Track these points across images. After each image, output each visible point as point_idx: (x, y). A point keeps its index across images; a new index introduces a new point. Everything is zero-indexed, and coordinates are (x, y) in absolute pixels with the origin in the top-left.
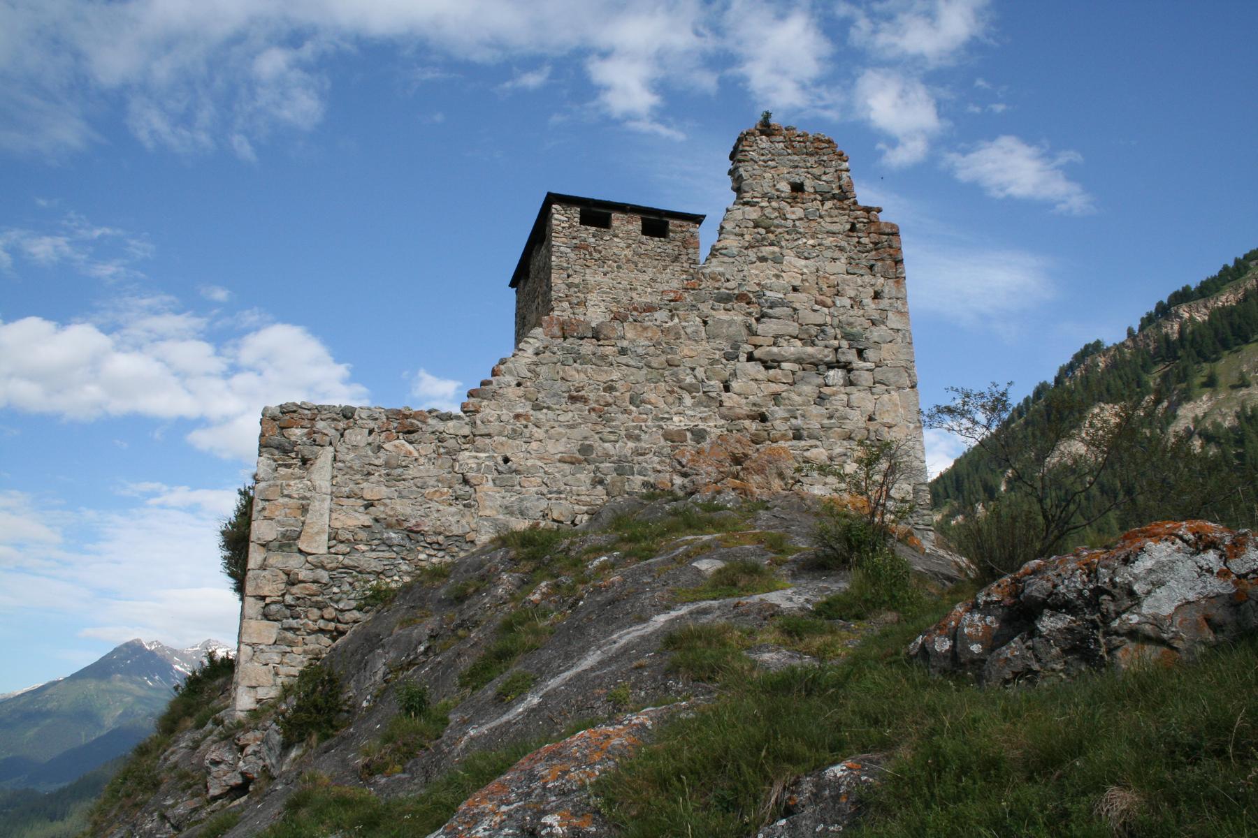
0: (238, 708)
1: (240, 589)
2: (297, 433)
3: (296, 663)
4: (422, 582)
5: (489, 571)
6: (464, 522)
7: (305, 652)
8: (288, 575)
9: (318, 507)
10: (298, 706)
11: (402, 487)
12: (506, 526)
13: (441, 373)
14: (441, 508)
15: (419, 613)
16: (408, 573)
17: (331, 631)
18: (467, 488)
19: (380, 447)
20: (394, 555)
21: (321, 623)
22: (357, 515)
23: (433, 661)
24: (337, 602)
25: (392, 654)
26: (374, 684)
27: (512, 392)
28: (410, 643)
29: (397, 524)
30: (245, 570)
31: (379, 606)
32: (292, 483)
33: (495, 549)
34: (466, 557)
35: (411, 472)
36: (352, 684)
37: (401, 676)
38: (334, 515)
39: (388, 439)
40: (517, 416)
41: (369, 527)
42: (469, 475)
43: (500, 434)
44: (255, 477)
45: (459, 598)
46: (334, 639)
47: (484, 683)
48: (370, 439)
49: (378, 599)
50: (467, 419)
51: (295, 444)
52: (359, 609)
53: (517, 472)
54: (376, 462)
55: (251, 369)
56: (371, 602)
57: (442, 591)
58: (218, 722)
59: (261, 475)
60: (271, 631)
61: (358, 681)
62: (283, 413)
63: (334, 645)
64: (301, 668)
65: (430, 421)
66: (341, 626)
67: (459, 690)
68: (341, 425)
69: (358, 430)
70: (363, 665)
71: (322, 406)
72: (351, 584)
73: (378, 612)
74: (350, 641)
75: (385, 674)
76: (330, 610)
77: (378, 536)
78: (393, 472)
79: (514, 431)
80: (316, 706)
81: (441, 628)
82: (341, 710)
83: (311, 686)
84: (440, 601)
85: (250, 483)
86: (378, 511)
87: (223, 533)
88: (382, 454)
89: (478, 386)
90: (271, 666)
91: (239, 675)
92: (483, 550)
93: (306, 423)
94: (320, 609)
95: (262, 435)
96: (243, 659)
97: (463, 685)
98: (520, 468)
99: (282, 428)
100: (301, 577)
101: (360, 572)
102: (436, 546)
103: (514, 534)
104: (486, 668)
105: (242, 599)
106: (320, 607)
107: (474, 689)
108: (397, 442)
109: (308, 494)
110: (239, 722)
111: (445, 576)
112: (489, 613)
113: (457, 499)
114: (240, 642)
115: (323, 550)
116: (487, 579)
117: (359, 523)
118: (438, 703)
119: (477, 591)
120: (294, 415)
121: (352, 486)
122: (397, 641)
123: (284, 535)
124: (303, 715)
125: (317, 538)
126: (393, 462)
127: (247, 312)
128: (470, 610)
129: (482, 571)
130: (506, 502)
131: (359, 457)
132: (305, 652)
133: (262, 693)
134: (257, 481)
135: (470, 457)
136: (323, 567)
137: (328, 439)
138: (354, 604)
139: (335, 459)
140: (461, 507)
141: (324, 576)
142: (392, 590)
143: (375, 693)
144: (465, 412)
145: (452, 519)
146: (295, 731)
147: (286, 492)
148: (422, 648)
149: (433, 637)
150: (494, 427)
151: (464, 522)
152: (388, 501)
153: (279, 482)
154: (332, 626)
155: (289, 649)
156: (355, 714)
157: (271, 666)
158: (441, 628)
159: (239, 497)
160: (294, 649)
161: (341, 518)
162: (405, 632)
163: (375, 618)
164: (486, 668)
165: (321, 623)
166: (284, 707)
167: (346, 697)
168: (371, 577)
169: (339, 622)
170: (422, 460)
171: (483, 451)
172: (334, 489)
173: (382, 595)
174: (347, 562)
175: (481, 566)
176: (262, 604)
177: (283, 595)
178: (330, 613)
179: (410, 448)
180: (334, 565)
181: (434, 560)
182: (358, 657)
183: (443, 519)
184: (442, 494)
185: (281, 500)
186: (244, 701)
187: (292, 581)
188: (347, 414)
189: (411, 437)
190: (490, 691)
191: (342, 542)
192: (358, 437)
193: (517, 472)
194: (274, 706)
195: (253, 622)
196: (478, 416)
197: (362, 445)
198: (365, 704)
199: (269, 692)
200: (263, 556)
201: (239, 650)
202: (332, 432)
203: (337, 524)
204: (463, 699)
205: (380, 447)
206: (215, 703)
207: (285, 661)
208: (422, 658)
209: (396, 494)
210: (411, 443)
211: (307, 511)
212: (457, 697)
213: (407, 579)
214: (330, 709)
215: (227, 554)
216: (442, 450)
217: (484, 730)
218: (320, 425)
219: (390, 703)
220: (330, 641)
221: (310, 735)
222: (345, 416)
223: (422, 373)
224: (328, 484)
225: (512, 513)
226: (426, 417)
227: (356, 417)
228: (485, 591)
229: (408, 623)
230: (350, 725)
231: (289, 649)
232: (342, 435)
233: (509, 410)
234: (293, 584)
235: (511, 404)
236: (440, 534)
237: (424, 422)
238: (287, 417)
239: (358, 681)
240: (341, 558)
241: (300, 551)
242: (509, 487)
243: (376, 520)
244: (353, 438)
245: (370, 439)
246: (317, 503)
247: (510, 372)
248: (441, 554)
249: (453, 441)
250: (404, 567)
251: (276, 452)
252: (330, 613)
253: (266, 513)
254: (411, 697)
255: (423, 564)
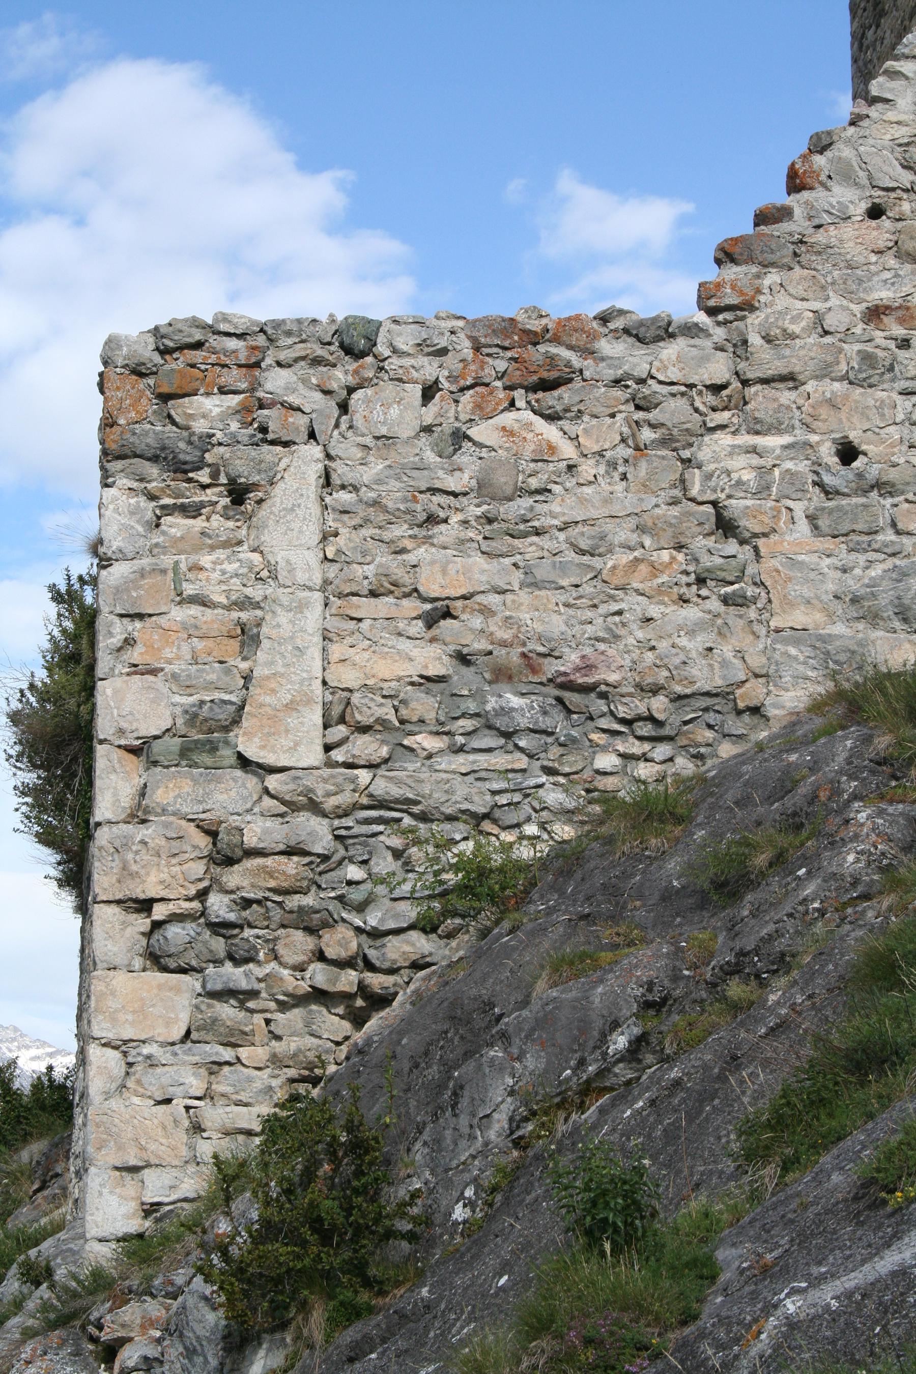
0: (92, 1231)
1: (76, 877)
2: (209, 411)
3: (250, 1098)
4: (609, 841)
5: (813, 799)
6: (726, 651)
7: (276, 1060)
8: (213, 834)
9: (286, 630)
10: (266, 1223)
11: (532, 553)
12: (856, 655)
13: (624, 178)
14: (654, 611)
15: (607, 934)
16: (567, 814)
17: (346, 997)
18: (732, 547)
19: (459, 438)
20: (522, 762)
21: (319, 975)
22: (404, 645)
23: (655, 1080)
24: (361, 908)
25: (533, 1062)
26: (482, 1153)
27: (856, 238)
28: (584, 1026)
29: (523, 665)
30: (87, 829)
31: (486, 917)
32: (206, 560)
33: (828, 731)
34: (741, 759)
35: (559, 508)
36: (419, 1153)
37: (561, 1128)
38: (337, 651)
39: (483, 413)
40: (875, 314)
41: (440, 679)
42: (736, 506)
43: (824, 373)
44: (95, 547)
45: (727, 886)
46: (358, 1020)
47: (817, 1148)
48: (429, 414)
49: (481, 895)
50: (719, 333)
51: (206, 442)
52: (427, 926)
53: (883, 487)
54: (452, 483)
55: (50, 208)
56: (461, 905)
57: (673, 865)
58: (38, 1275)
59: (114, 543)
60: (170, 1003)
61: (437, 1144)
62: (164, 352)
63: (359, 1037)
64: (266, 1109)
65: (606, 347)
66: (376, 981)
67: (740, 1171)
68: (340, 377)
69: (389, 389)
70: (447, 1097)
71: (278, 324)
72: (397, 854)
73: (484, 933)
74: (405, 1026)
75: (515, 1123)
76: (343, 932)
77: (472, 707)
78: (505, 514)
79: (867, 359)
80: (316, 1223)
81: (676, 977)
82: (390, 1234)
83: (299, 1163)
84: (667, 896)
85: (83, 565)
86: (465, 630)
87: (15, 718)
88: (466, 457)
89: (746, 228)
90: (179, 1104)
91: (87, 1134)
92: (792, 735)
93: (234, 377)
94: (310, 931)
95: (108, 423)
96: (96, 1085)
97: (754, 1155)
98: (892, 475)
99: (165, 398)
100: (251, 840)
101: (423, 817)
102: (645, 729)
103: (884, 680)
104: (819, 1102)
105: (83, 909)
106: (312, 924)
107: (786, 1168)
108: (508, 419)
109: (256, 592)
110: (97, 1274)
111: (679, 820)
112: (819, 928)
113: (701, 581)
114: (83, 1038)
115: (313, 755)
116: (808, 824)
117: (412, 671)
118: (680, 1211)
119: (779, 860)
120: (197, 356)
121: (383, 558)
122: (544, 1022)
123: (192, 718)
124: (281, 1250)
125: (292, 721)
126: (503, 480)
127: (24, 30)
128: (760, 920)
129: (790, 802)
130: (852, 584)
131: (400, 471)
132: (276, 1060)
133: (157, 1187)
134: (105, 562)
135: (734, 451)
136: (314, 807)
137: (301, 421)
138: (410, 912)
139: (328, 483)
140: (714, 604)
141: (317, 832)
142: (521, 867)
143: (489, 1178)
144: (712, 312)
145: (692, 644)
146: (259, 1297)
147: (189, 589)
148: (620, 1041)
149: (654, 1006)
150: (805, 352)
151: (726, 651)
152: (493, 599)
153: (167, 561)
154: (348, 980)
155: (227, 1054)
156: (431, 1243)
157: (179, 1104)
158: (676, 977)
159: (52, 609)
160: (244, 1053)
161: (360, 657)
162: (570, 993)
163: (477, 954)
164: (819, 1102)
165: (319, 975)
166: (223, 1227)
167: (403, 1193)
168: (458, 831)
169: (370, 967)
170: (588, 469)
171: (775, 428)
172: (332, 571)
173: (494, 881)
174: (382, 787)
175: (786, 784)
176: (142, 923)
177: (202, 895)
178: (340, 941)
179: (551, 432)
180: (346, 798)
181: (644, 771)
182: (433, 1072)
183: (663, 646)
184: (656, 569)
185: (179, 614)
186: (108, 1212)
187: (225, 855)
188: (355, 342)
189: (550, 399)
190: (836, 1176)
191: (364, 729)
192: (391, 409)
193: (883, 487)
194: (194, 1225)
195: (120, 979)
196: (754, 320)
197: (406, 432)
198: (459, 1213)
199: (179, 1183)
200: (138, 782)
201: (82, 1054)
202: (313, 401)
203: (348, 677)
204: (755, 1196)
205: (459, 438)
206: (24, 1218)
207: (219, 1088)
208: (623, 1072)
209: (517, 577)
210: (552, 417)
211: (256, 640)
212: (737, 1190)
213: (565, 831)
214: (359, 1231)
215: (30, 777)
216: (647, 435)
217: (828, 1295)
218: (276, 381)
219: (534, 1206)
220: (346, 1026)
221: (304, 1307)
222: (348, 350)
223: (567, 183)
224: (313, 557)
225: (873, 618)
226: (593, 336)
227: (382, 349)
228: (805, 860)
229: (573, 966)
230: (420, 1274)
231: (227, 1054)
232: (344, 407)
233: (847, 294)
234: (230, 861)
235: (854, 275)
236: (655, 690)
237: (588, 352)
238: (178, 363)
239: (437, 1144)
240: (364, 776)
241: (244, 762)
242: (859, 538)
243: (463, 659)
244: (378, 414)
245: (429, 414)
246: (283, 618)
247: (847, 176)
248: (662, 751)
249: (681, 403)
250: (553, 797)
251: (153, 470)
252: (340, 941)
253: (136, 655)
254: (599, 1198)
255: (609, 783)
